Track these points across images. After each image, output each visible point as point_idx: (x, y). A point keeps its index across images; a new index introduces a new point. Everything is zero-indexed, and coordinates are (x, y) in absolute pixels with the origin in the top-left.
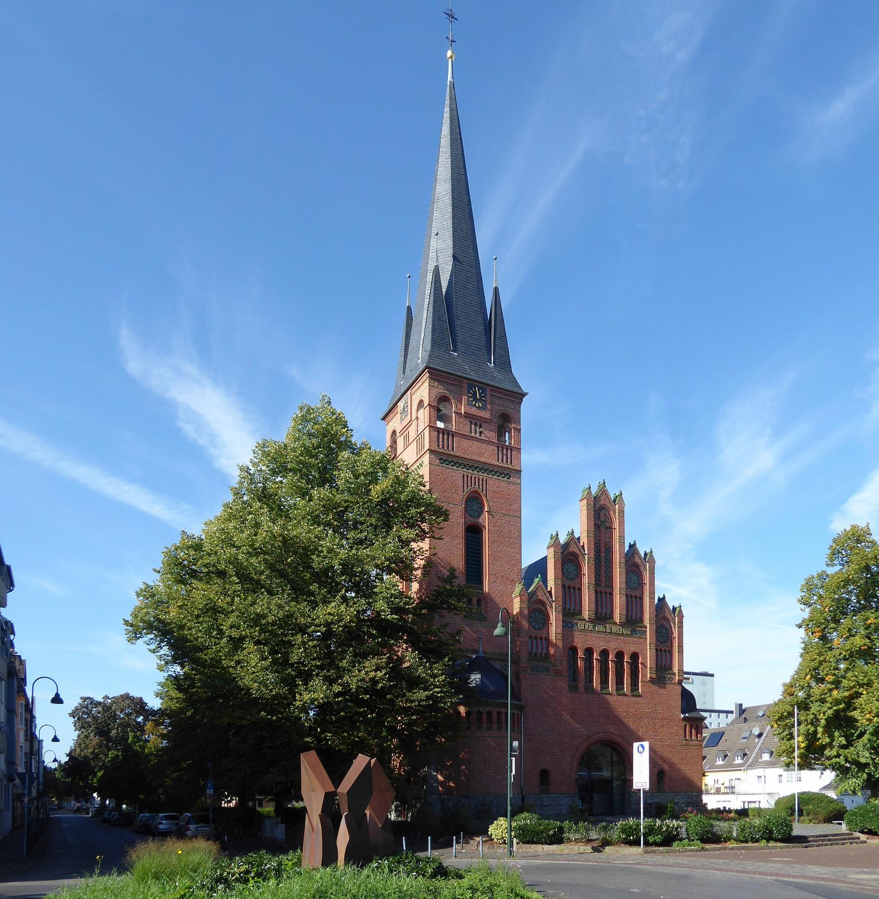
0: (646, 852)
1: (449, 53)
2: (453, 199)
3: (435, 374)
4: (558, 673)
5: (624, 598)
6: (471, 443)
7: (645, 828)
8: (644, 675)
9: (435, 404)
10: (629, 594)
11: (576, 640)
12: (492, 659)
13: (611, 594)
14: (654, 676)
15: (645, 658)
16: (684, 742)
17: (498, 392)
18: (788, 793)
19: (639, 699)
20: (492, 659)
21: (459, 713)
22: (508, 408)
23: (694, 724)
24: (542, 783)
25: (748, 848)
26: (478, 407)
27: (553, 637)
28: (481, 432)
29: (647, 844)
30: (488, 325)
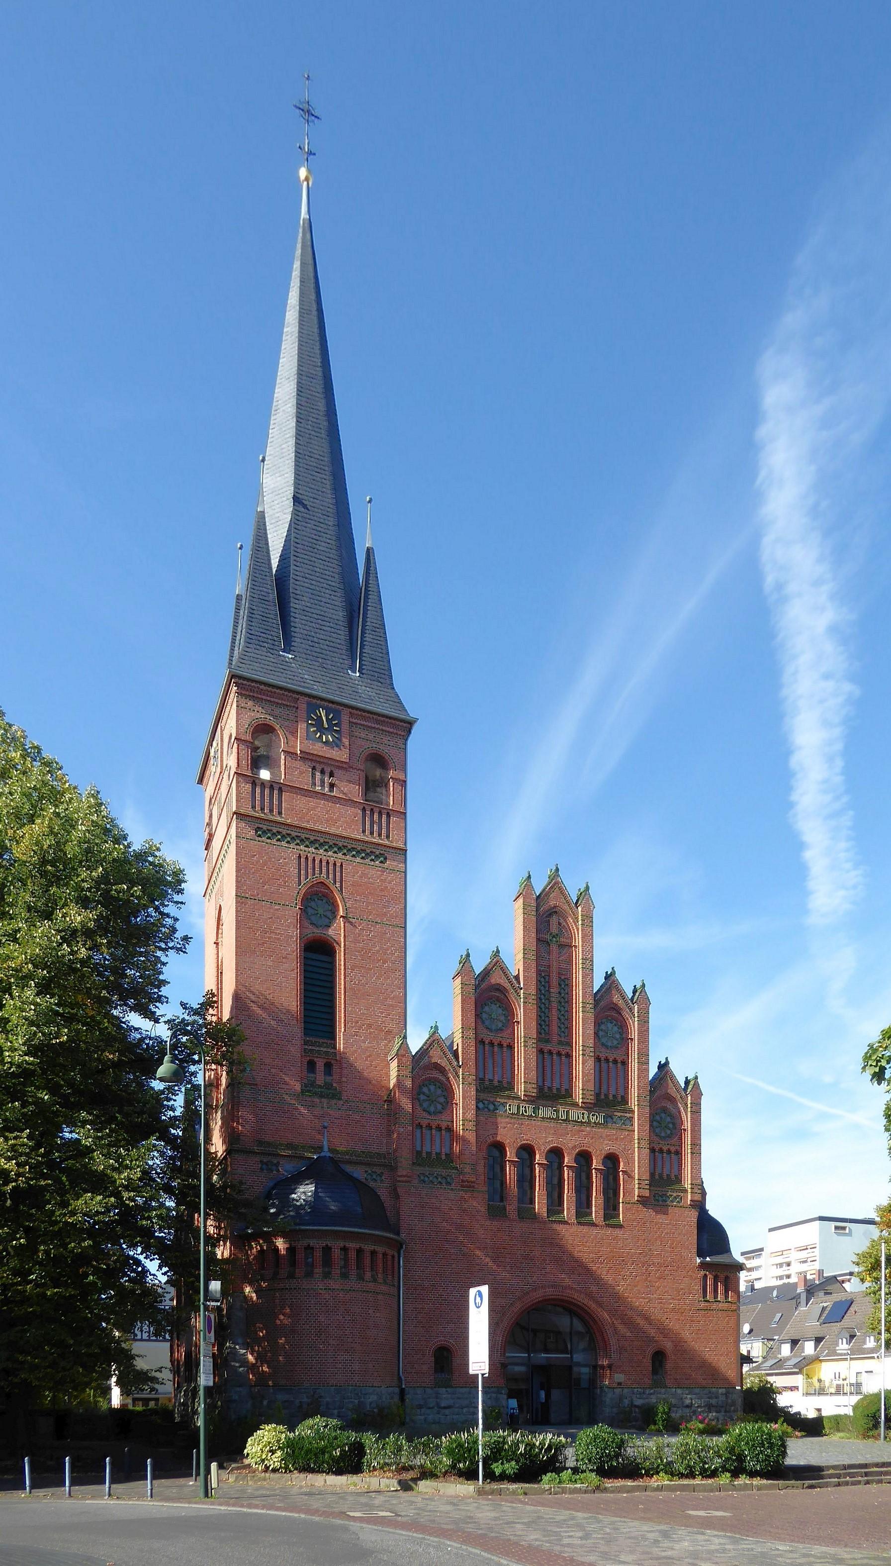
0: (480, 1492)
1: (303, 173)
2: (299, 405)
3: (246, 685)
4: (468, 1186)
5: (591, 1063)
6: (312, 802)
7: (485, 1446)
9: (248, 738)
10: (602, 1056)
11: (501, 1131)
12: (350, 1162)
13: (569, 1056)
14: (647, 1193)
15: (630, 1162)
18: (876, 1391)
19: (617, 1232)
20: (350, 1162)
21: (277, 1250)
22: (385, 746)
23: (722, 1276)
24: (655, 1371)
25: (694, 1488)
27: (459, 1126)
28: (332, 786)
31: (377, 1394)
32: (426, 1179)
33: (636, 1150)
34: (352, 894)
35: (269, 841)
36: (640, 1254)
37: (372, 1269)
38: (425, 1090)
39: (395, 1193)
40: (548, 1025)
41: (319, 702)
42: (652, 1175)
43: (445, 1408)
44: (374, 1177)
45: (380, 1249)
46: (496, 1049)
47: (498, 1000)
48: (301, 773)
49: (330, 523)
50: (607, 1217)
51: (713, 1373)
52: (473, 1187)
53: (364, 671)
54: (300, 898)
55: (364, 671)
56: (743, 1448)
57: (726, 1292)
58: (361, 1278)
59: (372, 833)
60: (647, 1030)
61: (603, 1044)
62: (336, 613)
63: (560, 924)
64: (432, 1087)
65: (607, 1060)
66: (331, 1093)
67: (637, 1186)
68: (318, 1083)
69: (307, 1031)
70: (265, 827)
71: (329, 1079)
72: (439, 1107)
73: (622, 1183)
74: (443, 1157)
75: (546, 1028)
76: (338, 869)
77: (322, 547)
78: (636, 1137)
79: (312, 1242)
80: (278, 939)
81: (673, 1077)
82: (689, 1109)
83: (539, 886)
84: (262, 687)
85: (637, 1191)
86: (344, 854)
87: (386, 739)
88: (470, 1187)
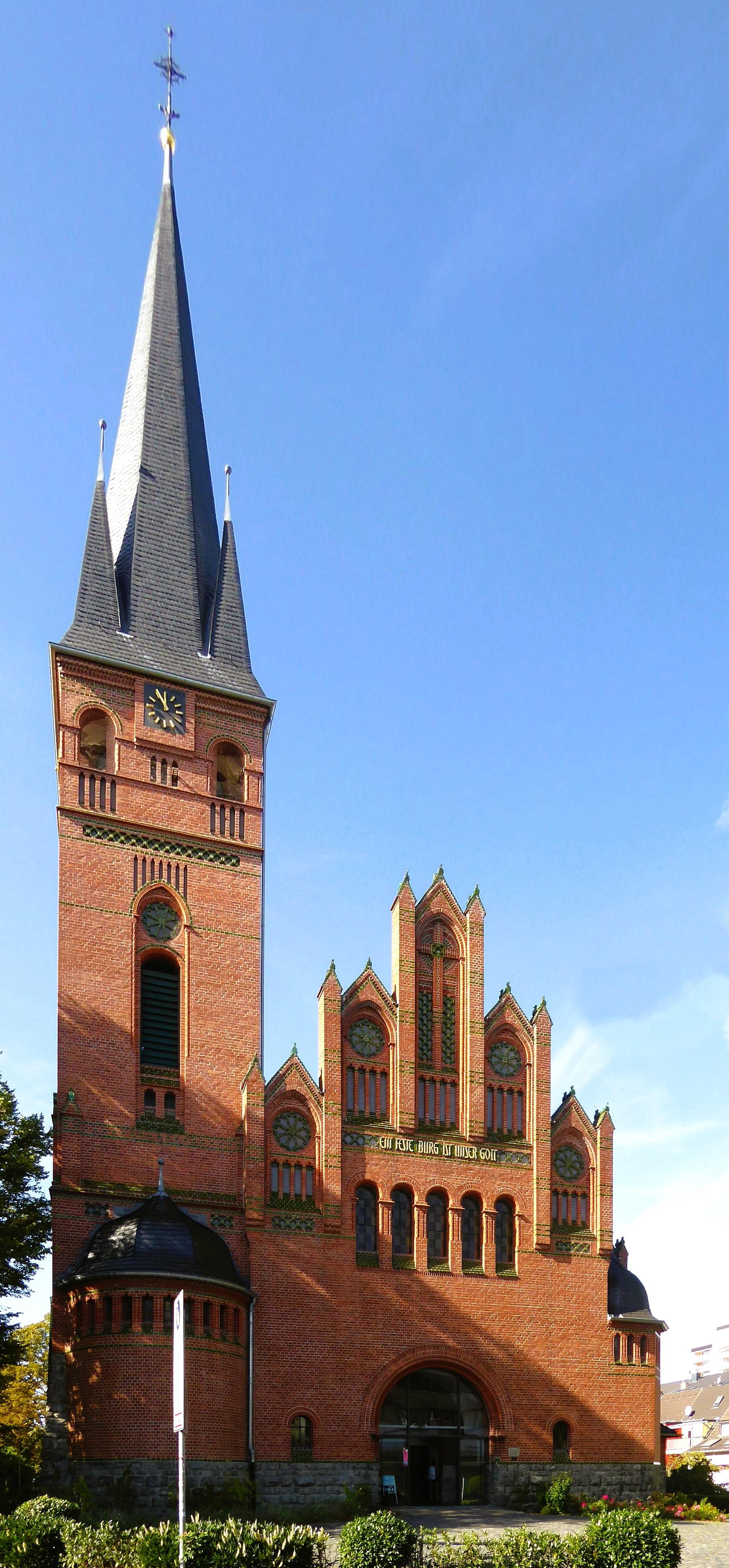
1: (164, 134)
4: (333, 1231)
5: (480, 1091)
6: (152, 796)
8: (525, 1239)
10: (496, 1084)
13: (455, 1084)
14: (547, 1241)
15: (527, 1204)
16: (615, 1368)
17: (214, 702)
19: (512, 1285)
20: (192, 1205)
23: (638, 1336)
26: (167, 729)
27: (320, 1162)
28: (175, 779)
31: (211, 1469)
32: (282, 1223)
33: (535, 1191)
34: (198, 900)
35: (99, 840)
36: (539, 1310)
37: (222, 1327)
38: (283, 1122)
39: (246, 1242)
40: (431, 1050)
41: (154, 682)
42: (554, 1221)
43: (303, 1486)
44: (222, 1222)
45: (217, 1301)
46: (368, 1075)
47: (371, 1020)
48: (138, 764)
49: (182, 497)
50: (499, 1268)
51: (624, 1444)
52: (339, 1233)
53: (215, 654)
54: (135, 905)
55: (215, 654)
56: (608, 1550)
57: (643, 1355)
58: (208, 1335)
59: (222, 833)
60: (548, 1055)
61: (496, 1072)
62: (186, 591)
63: (445, 935)
64: (292, 1120)
65: (501, 1089)
66: (172, 1127)
67: (535, 1232)
68: (158, 1115)
69: (144, 1058)
70: (94, 825)
71: (170, 1112)
72: (300, 1142)
73: (517, 1229)
74: (304, 1199)
75: (429, 1053)
76: (181, 873)
77: (171, 521)
78: (535, 1177)
79: (131, 1291)
80: (110, 952)
81: (578, 1109)
82: (599, 1146)
83: (419, 891)
84: (91, 666)
85: (535, 1237)
86: (189, 856)
87: (239, 726)
88: (334, 1232)
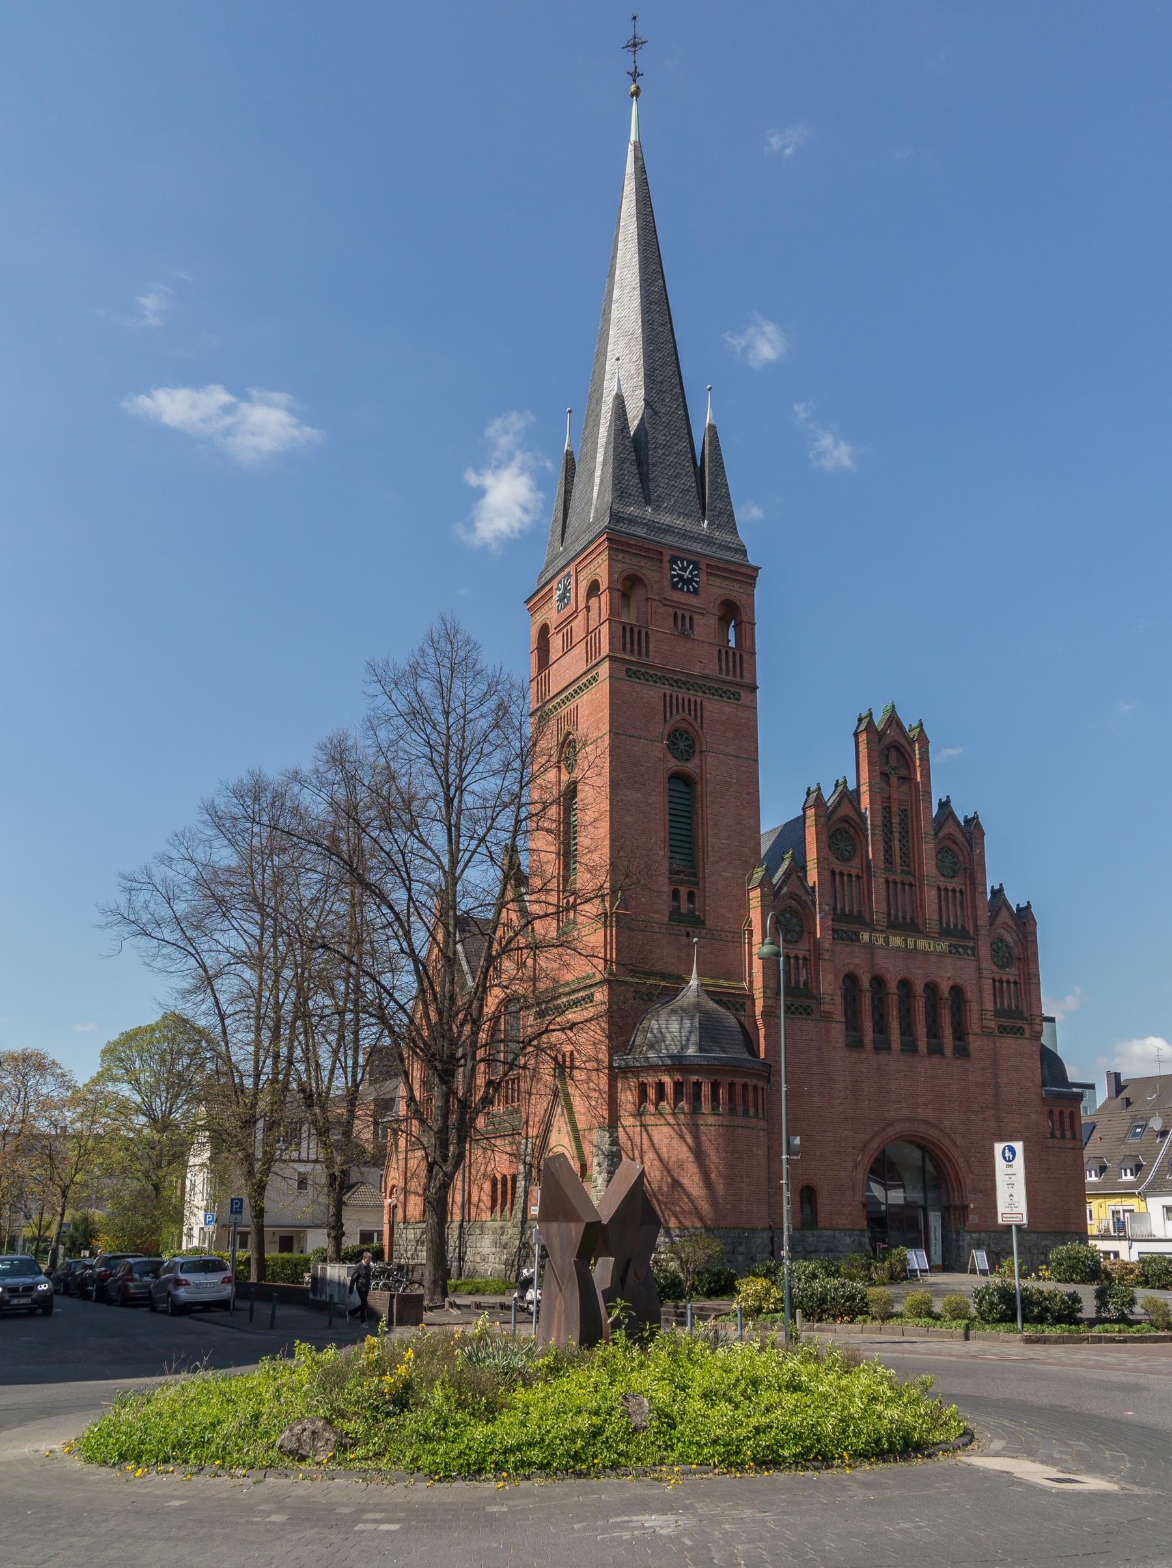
22: (734, 591)
29: (1025, 1320)
30: (699, 473)
72: (795, 935)
